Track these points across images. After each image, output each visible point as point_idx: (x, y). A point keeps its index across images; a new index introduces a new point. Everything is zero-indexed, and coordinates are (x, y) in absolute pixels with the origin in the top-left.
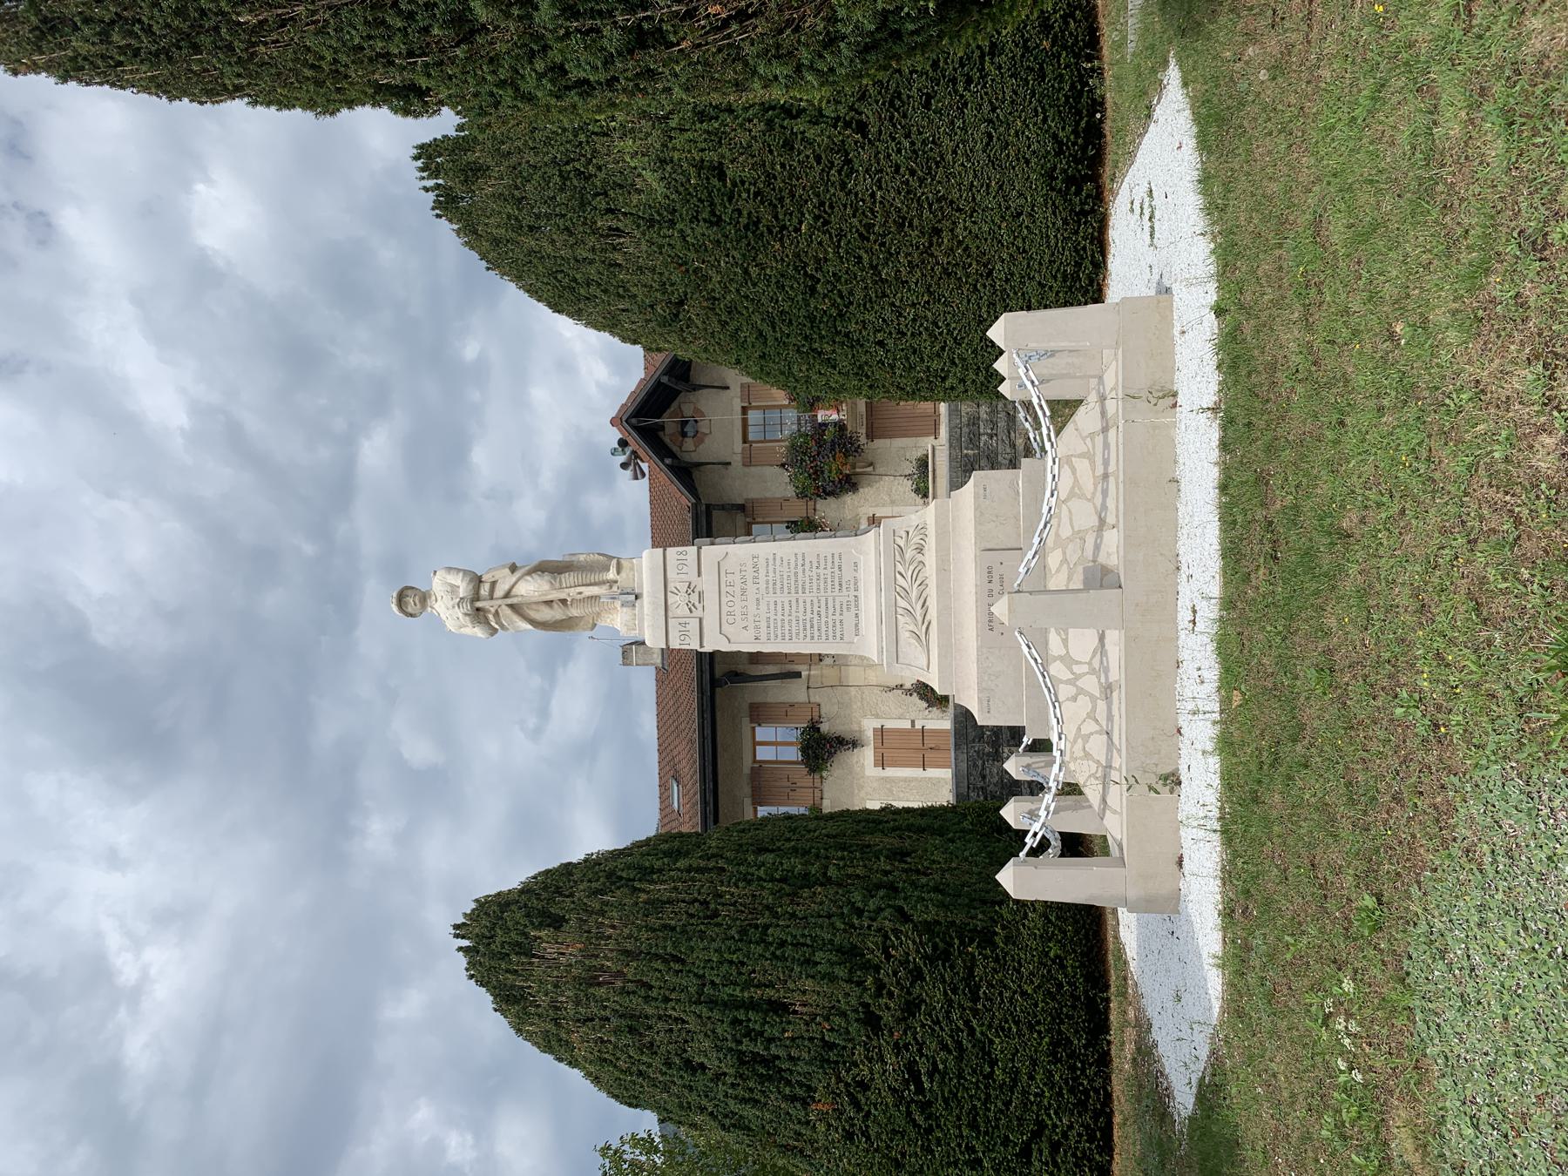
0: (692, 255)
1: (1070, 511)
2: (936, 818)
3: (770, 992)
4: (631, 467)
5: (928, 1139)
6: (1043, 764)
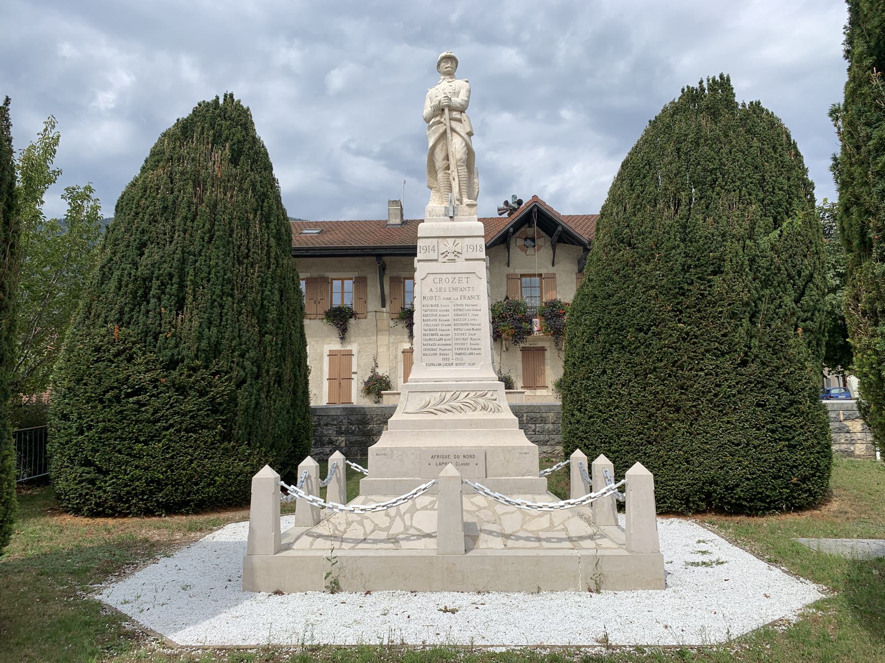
0: (663, 254)
1: (513, 513)
2: (302, 401)
3: (190, 299)
4: (505, 207)
5: (96, 400)
6: (338, 476)
